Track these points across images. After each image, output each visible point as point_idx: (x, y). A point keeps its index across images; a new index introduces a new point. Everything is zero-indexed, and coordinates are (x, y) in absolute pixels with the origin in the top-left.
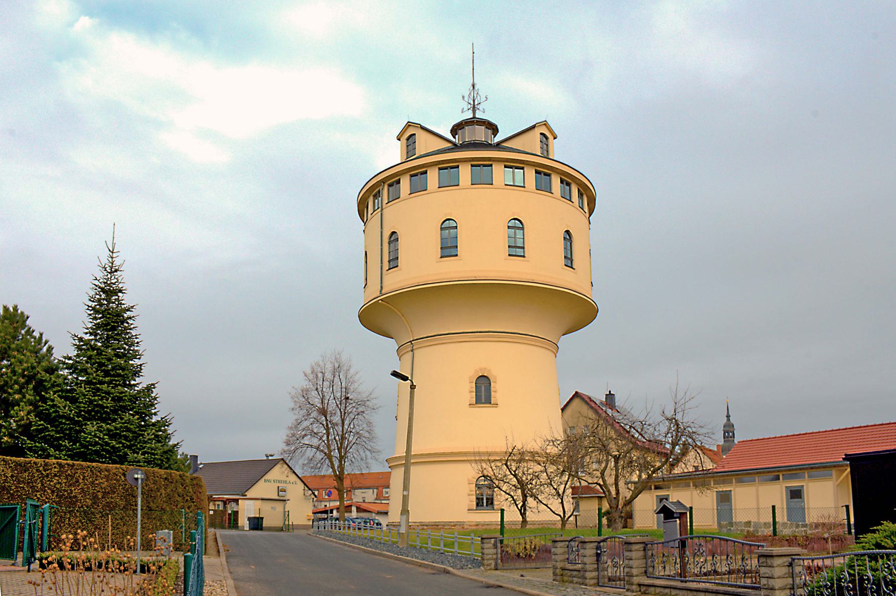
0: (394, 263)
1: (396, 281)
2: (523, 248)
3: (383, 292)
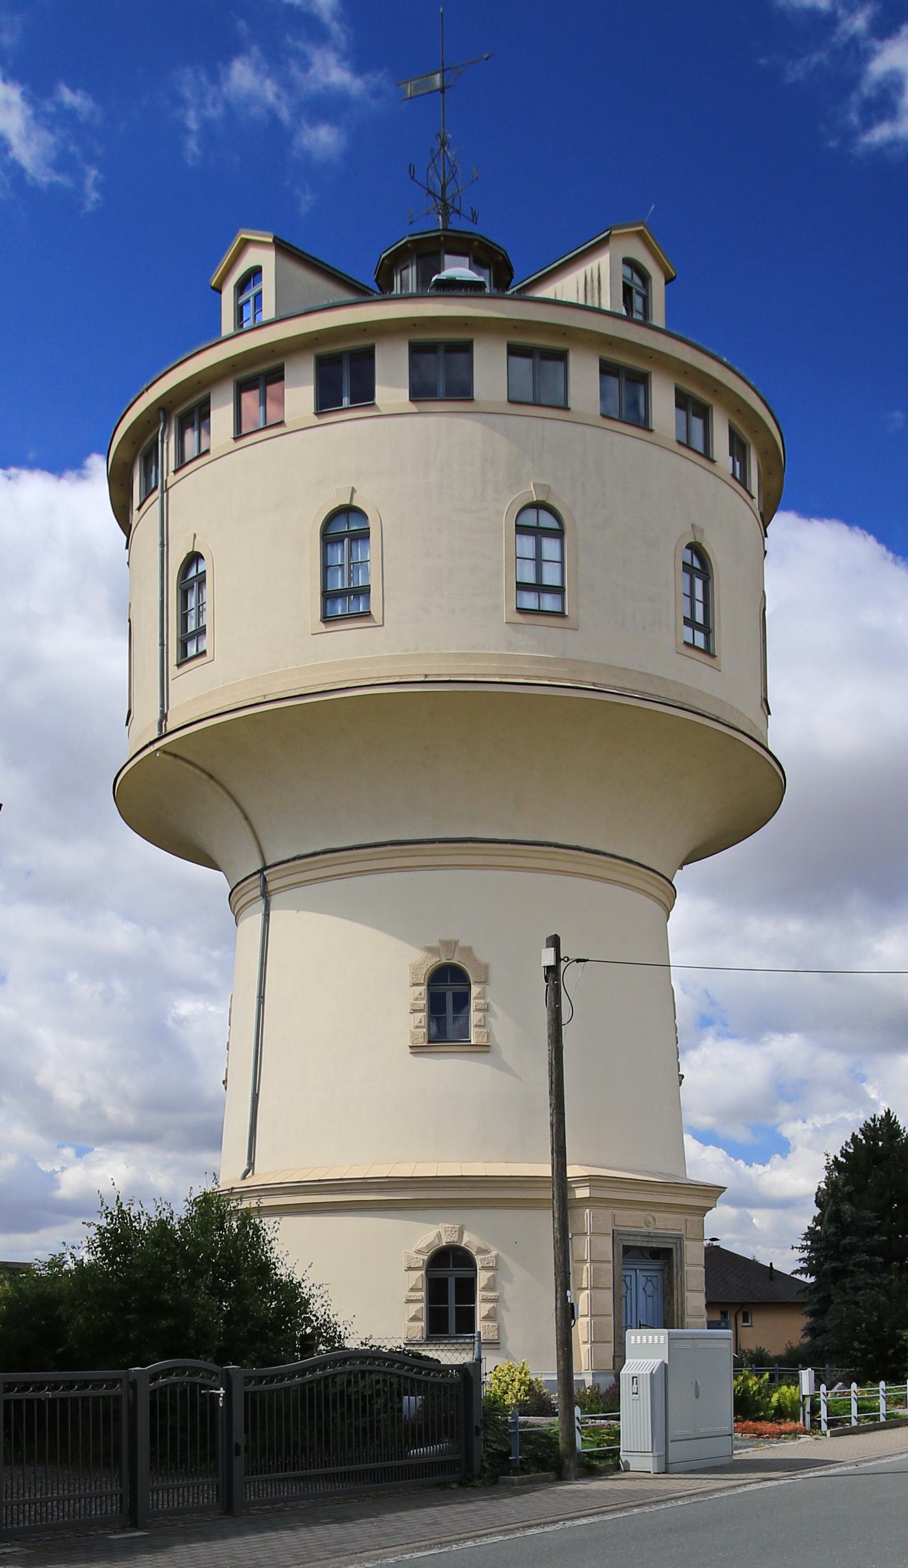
0: (188, 641)
1: (204, 693)
3: (171, 725)
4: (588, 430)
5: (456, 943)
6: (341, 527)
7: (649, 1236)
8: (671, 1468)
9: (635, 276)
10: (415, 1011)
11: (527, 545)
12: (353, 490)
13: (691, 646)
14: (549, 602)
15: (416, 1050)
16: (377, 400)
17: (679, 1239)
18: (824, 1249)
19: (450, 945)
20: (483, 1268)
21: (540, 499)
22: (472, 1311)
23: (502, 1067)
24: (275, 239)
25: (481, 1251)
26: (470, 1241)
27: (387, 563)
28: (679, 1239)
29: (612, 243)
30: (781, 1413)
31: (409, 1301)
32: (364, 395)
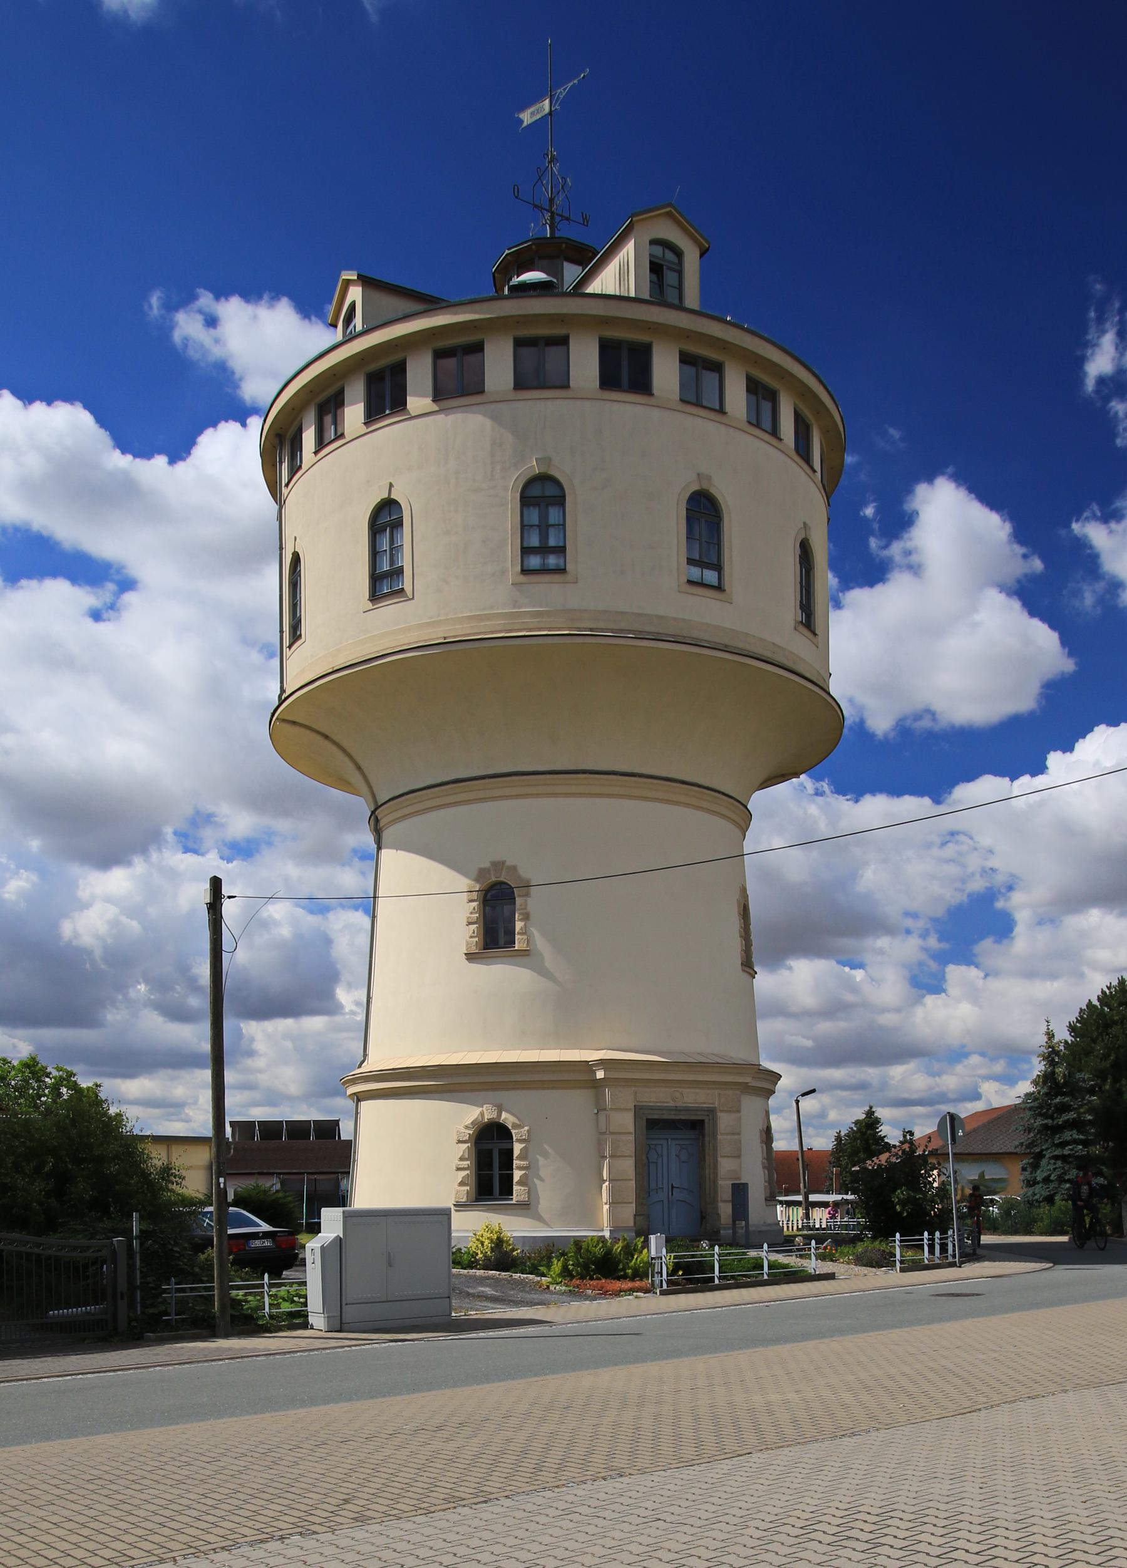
2: (718, 567)
4: (588, 404)
5: (503, 863)
6: (384, 519)
7: (676, 1109)
8: (345, 1327)
9: (667, 252)
10: (470, 923)
11: (534, 516)
12: (391, 485)
13: (701, 584)
14: (552, 561)
15: (470, 957)
16: (408, 406)
17: (712, 1112)
18: (1038, 1108)
19: (498, 865)
20: (518, 1140)
21: (542, 471)
22: (511, 1176)
23: (541, 970)
24: (359, 276)
25: (515, 1126)
26: (507, 1118)
27: (420, 548)
28: (712, 1112)
29: (637, 227)
30: (639, 1274)
31: (458, 1169)
32: (399, 404)
